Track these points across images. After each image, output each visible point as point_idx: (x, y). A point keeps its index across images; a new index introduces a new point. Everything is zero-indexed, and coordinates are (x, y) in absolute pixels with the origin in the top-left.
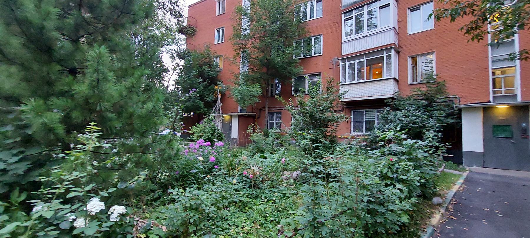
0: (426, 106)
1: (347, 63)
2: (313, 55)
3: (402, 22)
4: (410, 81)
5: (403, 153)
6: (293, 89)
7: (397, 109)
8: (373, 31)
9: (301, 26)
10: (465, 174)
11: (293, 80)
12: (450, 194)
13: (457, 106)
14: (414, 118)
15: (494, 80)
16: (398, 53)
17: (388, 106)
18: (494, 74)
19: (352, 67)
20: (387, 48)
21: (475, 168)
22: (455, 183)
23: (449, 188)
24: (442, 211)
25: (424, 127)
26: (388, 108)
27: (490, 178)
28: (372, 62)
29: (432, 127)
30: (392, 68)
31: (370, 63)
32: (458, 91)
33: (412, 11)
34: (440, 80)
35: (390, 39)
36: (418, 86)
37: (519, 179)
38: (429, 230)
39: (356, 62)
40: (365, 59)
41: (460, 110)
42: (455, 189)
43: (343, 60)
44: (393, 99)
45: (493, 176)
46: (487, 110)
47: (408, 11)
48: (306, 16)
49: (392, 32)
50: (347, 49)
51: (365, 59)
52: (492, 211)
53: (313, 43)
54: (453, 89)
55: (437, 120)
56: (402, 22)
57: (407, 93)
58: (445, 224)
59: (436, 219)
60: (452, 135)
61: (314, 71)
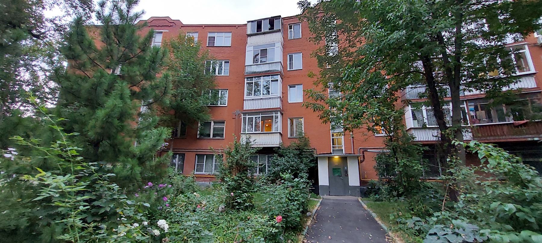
0: (299, 154)
1: (247, 117)
2: (219, 105)
3: (285, 93)
4: (289, 136)
5: (293, 187)
6: (198, 133)
7: (281, 156)
8: (268, 96)
9: (212, 79)
10: (321, 200)
11: (199, 125)
12: (314, 211)
13: (315, 155)
14: (293, 163)
15: (333, 139)
16: (282, 114)
17: (276, 153)
18: (333, 135)
19: (251, 120)
20: (275, 110)
21: (325, 197)
22: (316, 206)
23: (313, 209)
24: (312, 219)
25: (298, 169)
26: (276, 155)
27: (332, 201)
28: (266, 118)
29: (303, 170)
30: (278, 126)
31: (263, 119)
32: (317, 145)
33: (290, 87)
34: (306, 137)
35: (277, 104)
36: (295, 140)
37: (344, 200)
38: (307, 227)
39: (254, 117)
40: (260, 116)
41: (317, 158)
42: (316, 208)
43: (245, 114)
44: (279, 148)
45: (333, 200)
46: (330, 159)
47: (288, 87)
48: (215, 71)
49: (279, 99)
50: (248, 106)
51: (260, 116)
52: (332, 217)
53: (220, 96)
54: (314, 144)
55: (305, 164)
56: (285, 93)
57: (288, 144)
58: (312, 225)
59: (309, 223)
60: (313, 174)
61: (219, 119)
